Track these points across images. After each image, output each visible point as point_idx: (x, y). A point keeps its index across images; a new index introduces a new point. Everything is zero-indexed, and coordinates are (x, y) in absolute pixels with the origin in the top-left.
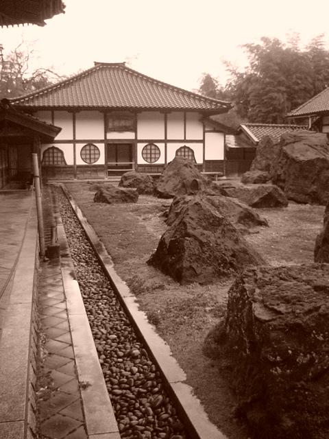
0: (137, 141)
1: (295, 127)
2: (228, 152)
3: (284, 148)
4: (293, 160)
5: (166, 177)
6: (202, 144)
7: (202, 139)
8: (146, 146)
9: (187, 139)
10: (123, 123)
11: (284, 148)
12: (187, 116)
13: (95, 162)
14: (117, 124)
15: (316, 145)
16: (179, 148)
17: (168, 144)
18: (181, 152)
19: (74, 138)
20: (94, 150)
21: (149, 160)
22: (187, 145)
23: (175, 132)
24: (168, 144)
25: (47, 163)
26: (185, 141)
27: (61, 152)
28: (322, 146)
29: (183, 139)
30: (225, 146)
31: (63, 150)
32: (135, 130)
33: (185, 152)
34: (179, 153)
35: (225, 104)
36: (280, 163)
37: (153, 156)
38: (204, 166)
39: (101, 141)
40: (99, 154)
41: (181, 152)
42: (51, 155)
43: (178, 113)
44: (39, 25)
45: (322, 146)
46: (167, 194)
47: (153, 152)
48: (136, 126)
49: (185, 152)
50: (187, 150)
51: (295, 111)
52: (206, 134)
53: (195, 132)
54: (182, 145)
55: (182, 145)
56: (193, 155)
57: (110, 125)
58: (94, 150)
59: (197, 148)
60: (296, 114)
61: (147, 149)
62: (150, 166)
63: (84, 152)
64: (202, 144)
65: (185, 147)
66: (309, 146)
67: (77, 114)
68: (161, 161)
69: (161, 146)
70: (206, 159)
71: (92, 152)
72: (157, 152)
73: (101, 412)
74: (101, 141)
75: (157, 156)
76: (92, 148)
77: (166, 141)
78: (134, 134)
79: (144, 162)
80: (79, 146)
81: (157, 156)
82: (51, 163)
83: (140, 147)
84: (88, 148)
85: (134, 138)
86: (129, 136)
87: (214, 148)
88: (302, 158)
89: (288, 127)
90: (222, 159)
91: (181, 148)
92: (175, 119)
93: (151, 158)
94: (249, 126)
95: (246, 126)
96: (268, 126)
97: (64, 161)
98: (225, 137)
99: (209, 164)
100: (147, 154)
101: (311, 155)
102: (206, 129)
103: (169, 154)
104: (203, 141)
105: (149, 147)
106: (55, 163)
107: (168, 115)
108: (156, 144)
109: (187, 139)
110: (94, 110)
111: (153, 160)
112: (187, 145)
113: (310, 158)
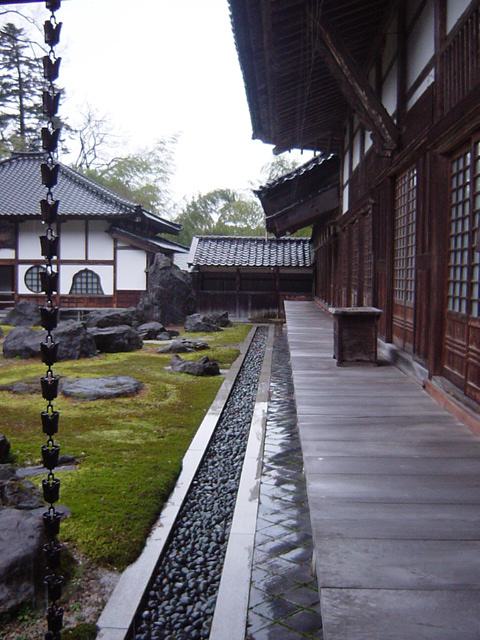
0: (17, 262)
6: (112, 267)
7: (112, 259)
12: (90, 225)
18: (81, 277)
19: (87, 257)
22: (90, 267)
26: (86, 262)
27: (98, 277)
29: (84, 259)
31: (99, 274)
32: (14, 246)
33: (85, 277)
38: (116, 299)
40: (25, 279)
41: (81, 277)
42: (84, 280)
47: (90, 280)
49: (85, 277)
50: (90, 275)
52: (119, 252)
53: (101, 248)
54: (83, 267)
55: (83, 267)
56: (98, 283)
59: (104, 273)
63: (29, 276)
64: (112, 267)
65: (86, 271)
70: (118, 289)
73: (467, 558)
78: (13, 252)
82: (84, 292)
83: (22, 270)
84: (35, 270)
85: (13, 257)
90: (145, 289)
91: (81, 272)
97: (101, 290)
99: (124, 297)
100: (32, 280)
102: (119, 245)
104: (113, 263)
106: (89, 292)
112: (90, 267)
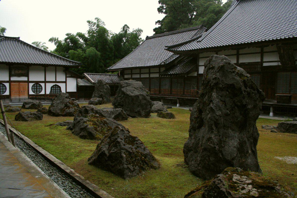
1: (111, 75)
2: (78, 87)
3: (122, 89)
4: (128, 95)
5: (56, 104)
6: (65, 84)
7: (64, 80)
8: (34, 85)
9: (57, 81)
10: (20, 72)
11: (122, 89)
13: (3, 93)
14: (17, 72)
15: (138, 88)
16: (52, 85)
17: (47, 84)
18: (54, 88)
20: (39, 86)
21: (36, 92)
22: (57, 84)
23: (51, 77)
24: (47, 84)
25: (53, 93)
26: (56, 82)
27: (60, 87)
28: (141, 88)
30: (77, 85)
31: (60, 86)
33: (56, 88)
34: (53, 89)
35: (78, 63)
36: (120, 96)
37: (38, 90)
39: (7, 82)
41: (54, 88)
43: (52, 67)
44: (80, 33)
45: (141, 88)
46: (58, 114)
48: (29, 73)
49: (56, 88)
51: (111, 67)
53: (61, 77)
54: (54, 84)
55: (54, 84)
57: (13, 73)
58: (39, 86)
59: (62, 86)
60: (112, 68)
61: (34, 86)
62: (37, 95)
64: (65, 84)
65: (56, 85)
66: (134, 88)
67: (47, 68)
68: (43, 93)
69: (43, 85)
71: (38, 88)
72: (40, 87)
74: (7, 82)
75: (40, 90)
76: (38, 85)
77: (45, 82)
79: (33, 94)
80: (31, 85)
81: (40, 90)
82: (55, 93)
86: (25, 79)
87: (71, 86)
88: (132, 95)
89: (107, 75)
91: (54, 85)
92: (51, 71)
93: (37, 91)
94: (88, 74)
95: (87, 74)
96: (98, 74)
98: (77, 80)
101: (137, 93)
102: (67, 76)
103: (47, 89)
104: (65, 82)
105: (35, 85)
106: (57, 93)
107: (47, 68)
108: (4, 84)
109: (57, 81)
110: (37, 65)
111: (38, 92)
112: (57, 84)
113: (136, 94)
